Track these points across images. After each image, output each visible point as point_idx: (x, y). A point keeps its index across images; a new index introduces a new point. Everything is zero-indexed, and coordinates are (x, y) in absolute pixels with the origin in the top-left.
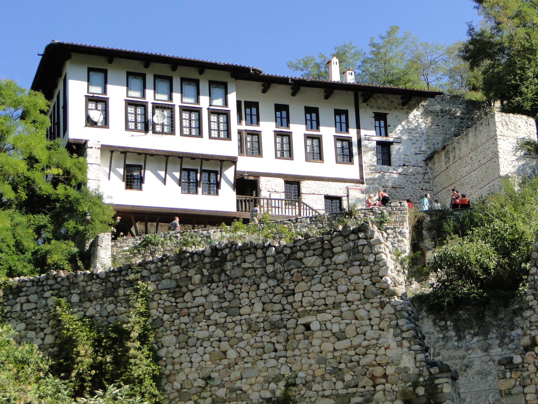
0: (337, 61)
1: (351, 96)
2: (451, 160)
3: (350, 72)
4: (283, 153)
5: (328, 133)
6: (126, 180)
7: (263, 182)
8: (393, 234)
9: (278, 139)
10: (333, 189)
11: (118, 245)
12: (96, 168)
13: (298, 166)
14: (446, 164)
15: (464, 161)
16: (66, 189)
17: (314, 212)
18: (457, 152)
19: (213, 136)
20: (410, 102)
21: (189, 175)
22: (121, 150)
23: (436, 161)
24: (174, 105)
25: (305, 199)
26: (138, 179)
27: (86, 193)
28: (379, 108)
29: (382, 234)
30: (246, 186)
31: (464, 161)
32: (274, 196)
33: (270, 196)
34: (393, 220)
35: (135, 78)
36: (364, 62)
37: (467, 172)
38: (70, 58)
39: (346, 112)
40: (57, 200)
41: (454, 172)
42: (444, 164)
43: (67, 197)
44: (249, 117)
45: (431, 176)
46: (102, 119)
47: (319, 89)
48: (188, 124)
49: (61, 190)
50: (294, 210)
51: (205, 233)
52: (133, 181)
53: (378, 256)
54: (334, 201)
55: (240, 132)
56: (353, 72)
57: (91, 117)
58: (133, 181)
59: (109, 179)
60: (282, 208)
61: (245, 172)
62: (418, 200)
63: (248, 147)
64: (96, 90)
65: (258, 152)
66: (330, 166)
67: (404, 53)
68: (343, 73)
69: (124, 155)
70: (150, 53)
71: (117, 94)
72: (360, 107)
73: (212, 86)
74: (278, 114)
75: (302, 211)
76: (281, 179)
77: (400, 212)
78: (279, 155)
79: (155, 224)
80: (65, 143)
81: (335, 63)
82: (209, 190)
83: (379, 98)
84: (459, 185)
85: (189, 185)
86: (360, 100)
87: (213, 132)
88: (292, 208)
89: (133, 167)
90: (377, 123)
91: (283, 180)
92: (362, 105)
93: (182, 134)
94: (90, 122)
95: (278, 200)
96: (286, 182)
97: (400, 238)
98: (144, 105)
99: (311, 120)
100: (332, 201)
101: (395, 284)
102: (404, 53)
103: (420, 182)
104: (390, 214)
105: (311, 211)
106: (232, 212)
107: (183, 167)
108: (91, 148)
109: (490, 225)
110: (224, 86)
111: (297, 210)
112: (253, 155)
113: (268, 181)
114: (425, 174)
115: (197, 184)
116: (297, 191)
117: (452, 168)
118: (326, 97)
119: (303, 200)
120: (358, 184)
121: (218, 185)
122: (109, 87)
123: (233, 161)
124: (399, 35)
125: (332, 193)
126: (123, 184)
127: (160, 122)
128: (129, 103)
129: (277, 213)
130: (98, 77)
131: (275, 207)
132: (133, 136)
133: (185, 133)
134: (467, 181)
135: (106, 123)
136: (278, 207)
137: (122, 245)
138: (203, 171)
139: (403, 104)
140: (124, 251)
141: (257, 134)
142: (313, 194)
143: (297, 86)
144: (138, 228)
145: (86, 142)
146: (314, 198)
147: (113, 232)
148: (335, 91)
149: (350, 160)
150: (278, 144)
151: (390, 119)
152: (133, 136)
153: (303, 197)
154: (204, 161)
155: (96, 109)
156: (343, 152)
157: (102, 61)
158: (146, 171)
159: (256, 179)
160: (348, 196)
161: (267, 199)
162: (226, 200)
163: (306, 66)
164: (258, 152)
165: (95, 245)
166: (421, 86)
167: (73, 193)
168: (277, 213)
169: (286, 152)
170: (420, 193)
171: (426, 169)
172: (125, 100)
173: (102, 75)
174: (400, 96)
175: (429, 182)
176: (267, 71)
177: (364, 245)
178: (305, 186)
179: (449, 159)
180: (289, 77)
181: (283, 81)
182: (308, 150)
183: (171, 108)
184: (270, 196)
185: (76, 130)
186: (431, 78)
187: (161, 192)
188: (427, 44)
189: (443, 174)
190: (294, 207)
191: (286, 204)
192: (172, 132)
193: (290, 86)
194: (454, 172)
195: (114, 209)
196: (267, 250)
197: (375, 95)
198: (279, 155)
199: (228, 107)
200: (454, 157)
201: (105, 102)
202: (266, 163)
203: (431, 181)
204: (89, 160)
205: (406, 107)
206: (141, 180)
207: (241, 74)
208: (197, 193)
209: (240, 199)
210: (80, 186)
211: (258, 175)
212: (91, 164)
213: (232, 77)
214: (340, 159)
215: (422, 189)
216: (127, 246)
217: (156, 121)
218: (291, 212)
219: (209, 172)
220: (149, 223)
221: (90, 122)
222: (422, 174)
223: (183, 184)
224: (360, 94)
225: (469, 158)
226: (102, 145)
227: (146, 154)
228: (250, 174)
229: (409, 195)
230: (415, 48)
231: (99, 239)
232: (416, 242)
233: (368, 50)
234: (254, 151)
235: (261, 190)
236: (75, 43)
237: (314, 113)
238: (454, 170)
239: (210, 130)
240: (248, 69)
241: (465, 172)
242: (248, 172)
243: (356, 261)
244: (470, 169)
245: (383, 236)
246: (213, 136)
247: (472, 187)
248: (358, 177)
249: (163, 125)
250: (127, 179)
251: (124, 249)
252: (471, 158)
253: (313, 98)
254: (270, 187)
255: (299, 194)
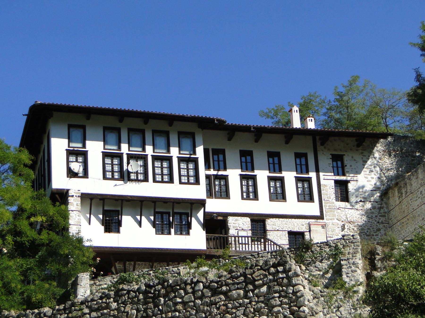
0: (298, 109)
1: (310, 139)
2: (404, 195)
3: (311, 118)
4: (249, 194)
5: (289, 177)
6: (104, 225)
7: (231, 220)
8: (347, 265)
9: (243, 182)
10: (296, 225)
11: (97, 284)
12: (77, 215)
13: (263, 205)
14: (399, 199)
15: (415, 196)
16: (49, 234)
17: (278, 247)
18: (409, 187)
19: (183, 181)
20: (364, 144)
21: (181, 219)
22: (99, 197)
23: (390, 196)
24: (147, 155)
25: (270, 236)
26: (115, 223)
27: (68, 237)
28: (335, 150)
29: (300, 267)
30: (216, 226)
31: (415, 196)
32: (242, 233)
33: (238, 234)
34: (347, 252)
35: (111, 132)
36: (330, 109)
37: (418, 205)
38: (52, 117)
39: (305, 155)
40: (43, 245)
41: (406, 206)
42: (397, 199)
43: (51, 241)
44: (216, 163)
45: (386, 210)
46: (81, 170)
47: (280, 135)
48: (160, 171)
49: (44, 236)
50: (259, 246)
51: (175, 269)
52: (112, 225)
53: (296, 287)
54: (297, 236)
55: (208, 177)
56: (313, 119)
57: (72, 168)
58: (112, 225)
59: (90, 224)
60: (248, 244)
61: (214, 213)
62: (375, 233)
63: (217, 190)
64: (77, 145)
65: (225, 194)
66: (292, 205)
67: (365, 100)
68: (303, 119)
69: (102, 201)
70: (67, 104)
71: (95, 148)
72: (318, 150)
73: (71, 130)
74: (243, 159)
75: (267, 246)
76: (248, 218)
77: (353, 244)
78: (245, 197)
79: (132, 263)
80: (48, 193)
81: (296, 111)
82: (163, 230)
83: (338, 144)
84: (411, 217)
85: (162, 228)
86: (318, 144)
87: (183, 178)
88: (258, 244)
89: (111, 211)
90: (335, 163)
91: (249, 219)
92: (320, 148)
93: (155, 181)
94: (71, 174)
95: (245, 237)
96: (252, 221)
97: (353, 268)
98: (120, 156)
99: (274, 164)
100: (295, 236)
101: (312, 313)
102: (365, 100)
103: (376, 216)
104: (344, 246)
105: (275, 246)
106: (202, 250)
107: (156, 210)
108: (73, 196)
109: (422, 255)
110: (192, 136)
111: (263, 246)
112: (221, 197)
113: (236, 220)
114: (380, 208)
115: (170, 225)
116: (262, 229)
117: (405, 202)
118: (287, 142)
119: (268, 237)
120: (319, 221)
121: (189, 226)
122: (88, 143)
123: (202, 203)
124: (360, 84)
125: (296, 229)
126: (103, 228)
127: (135, 170)
128: (105, 155)
129: (244, 249)
130: (77, 134)
131: (242, 244)
132: (116, 185)
133: (157, 180)
134: (419, 213)
135: (86, 175)
136: (245, 244)
137: (101, 283)
138: (174, 214)
139: (358, 146)
140: (102, 289)
141: (225, 178)
142: (278, 230)
143: (259, 133)
144: (117, 267)
145: (68, 190)
146: (278, 235)
147: (93, 272)
148: (294, 136)
149: (311, 200)
150: (244, 187)
151: (347, 160)
152: (116, 185)
153: (268, 234)
154: (175, 204)
155: (77, 161)
156: (304, 191)
157: (81, 120)
158: (123, 216)
159: (225, 218)
160: (310, 231)
161: (235, 237)
162: (196, 239)
163: (276, 115)
164: (225, 194)
165: (75, 284)
166: (382, 129)
167: (57, 238)
168: (244, 249)
169: (251, 193)
170: (377, 226)
171: (381, 204)
172: (102, 152)
173: (82, 130)
174: (355, 139)
175: (384, 216)
176: (231, 120)
177: (283, 278)
178: (270, 224)
179: (402, 194)
180: (252, 125)
181: (246, 129)
182: (272, 191)
183: (144, 158)
184: (238, 234)
185: (59, 180)
186: (389, 121)
187: (137, 234)
188: (384, 91)
189: (397, 208)
190: (259, 243)
191: (252, 241)
192: (146, 180)
193: (253, 134)
194: (406, 206)
195: (94, 251)
196: (195, 286)
197: (332, 139)
198: (245, 197)
199: (145, 152)
200: (406, 192)
201: (85, 154)
202: (234, 203)
203: (386, 215)
204: (70, 207)
205: (360, 148)
206: (119, 224)
207: (207, 125)
208: (169, 233)
209: (210, 237)
210: (64, 229)
211: (226, 215)
212: (72, 211)
213: (199, 127)
214: (274, 196)
215: (378, 223)
216: (105, 284)
217: (130, 170)
218: (256, 248)
219: (181, 214)
220: (128, 263)
221: (71, 174)
222: (378, 208)
223: (157, 225)
224: (317, 138)
225: (419, 192)
226: (82, 194)
227: (122, 200)
228: (219, 214)
229: (366, 228)
230: (373, 95)
231: (79, 279)
232: (369, 271)
233: (332, 97)
234: (222, 194)
235: (229, 229)
236: (103, 107)
237: (276, 157)
238: (406, 204)
239: (180, 176)
240: (213, 120)
241: (416, 205)
242: (216, 213)
243: (275, 293)
244: (421, 203)
245: (301, 269)
246: (183, 181)
247: (423, 219)
248: (318, 214)
249: (137, 173)
250: (106, 223)
251: (102, 286)
252: (421, 192)
253: (275, 143)
254: (237, 225)
255: (265, 231)
